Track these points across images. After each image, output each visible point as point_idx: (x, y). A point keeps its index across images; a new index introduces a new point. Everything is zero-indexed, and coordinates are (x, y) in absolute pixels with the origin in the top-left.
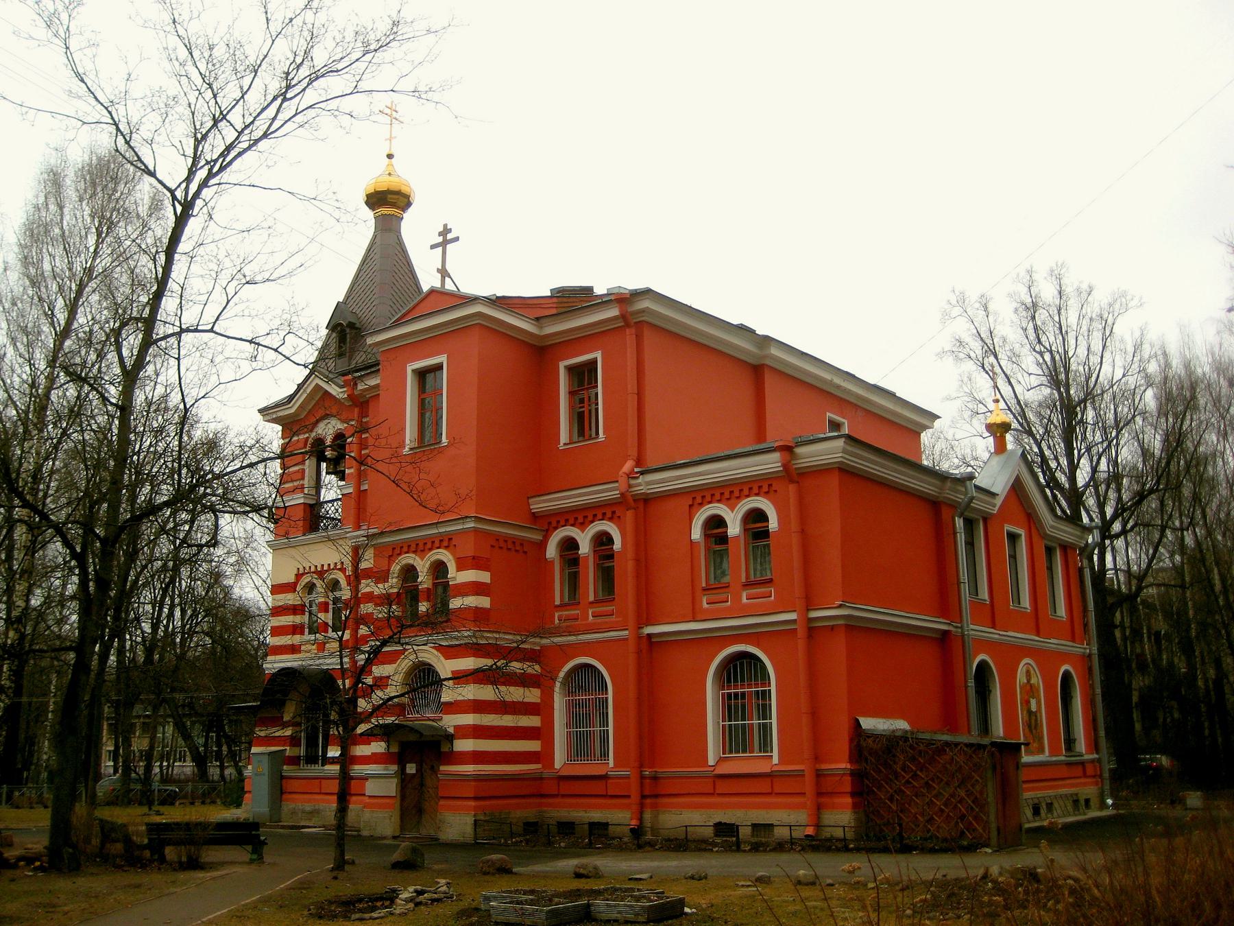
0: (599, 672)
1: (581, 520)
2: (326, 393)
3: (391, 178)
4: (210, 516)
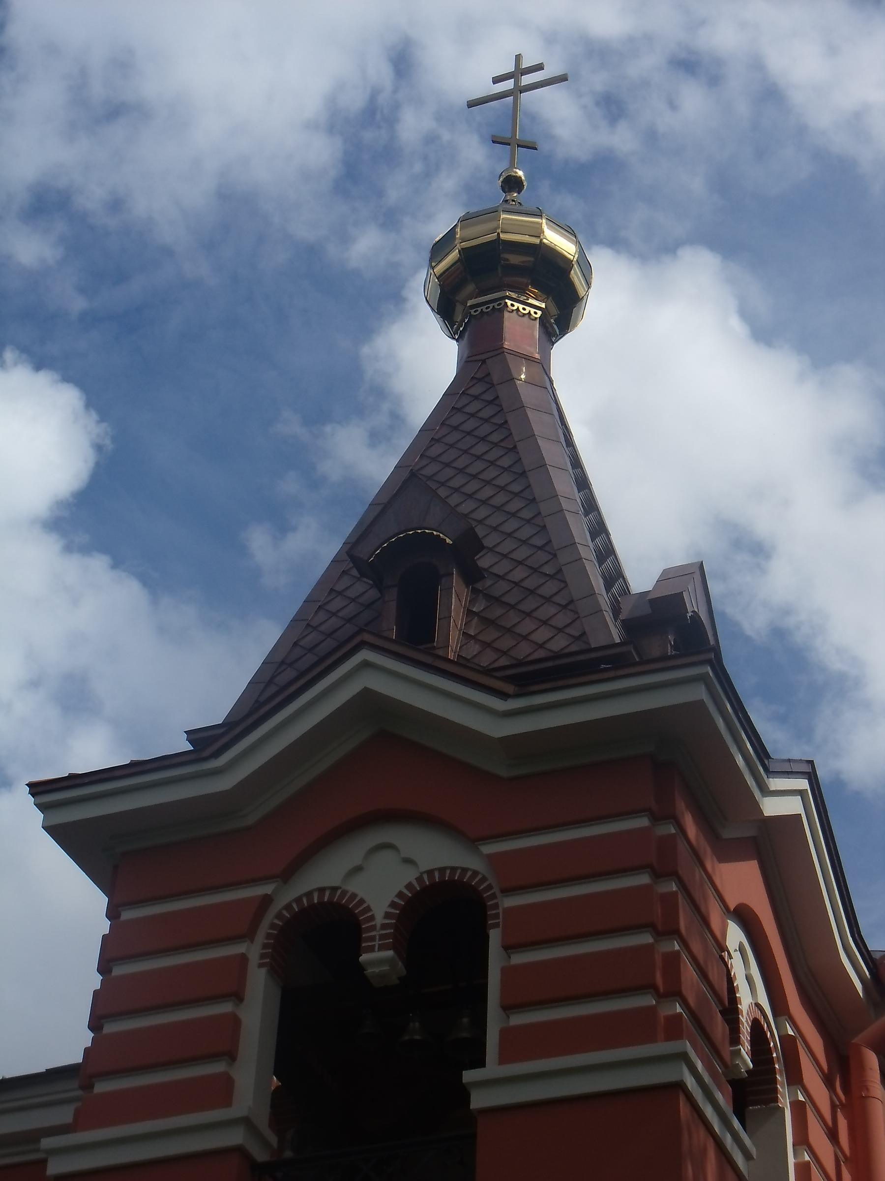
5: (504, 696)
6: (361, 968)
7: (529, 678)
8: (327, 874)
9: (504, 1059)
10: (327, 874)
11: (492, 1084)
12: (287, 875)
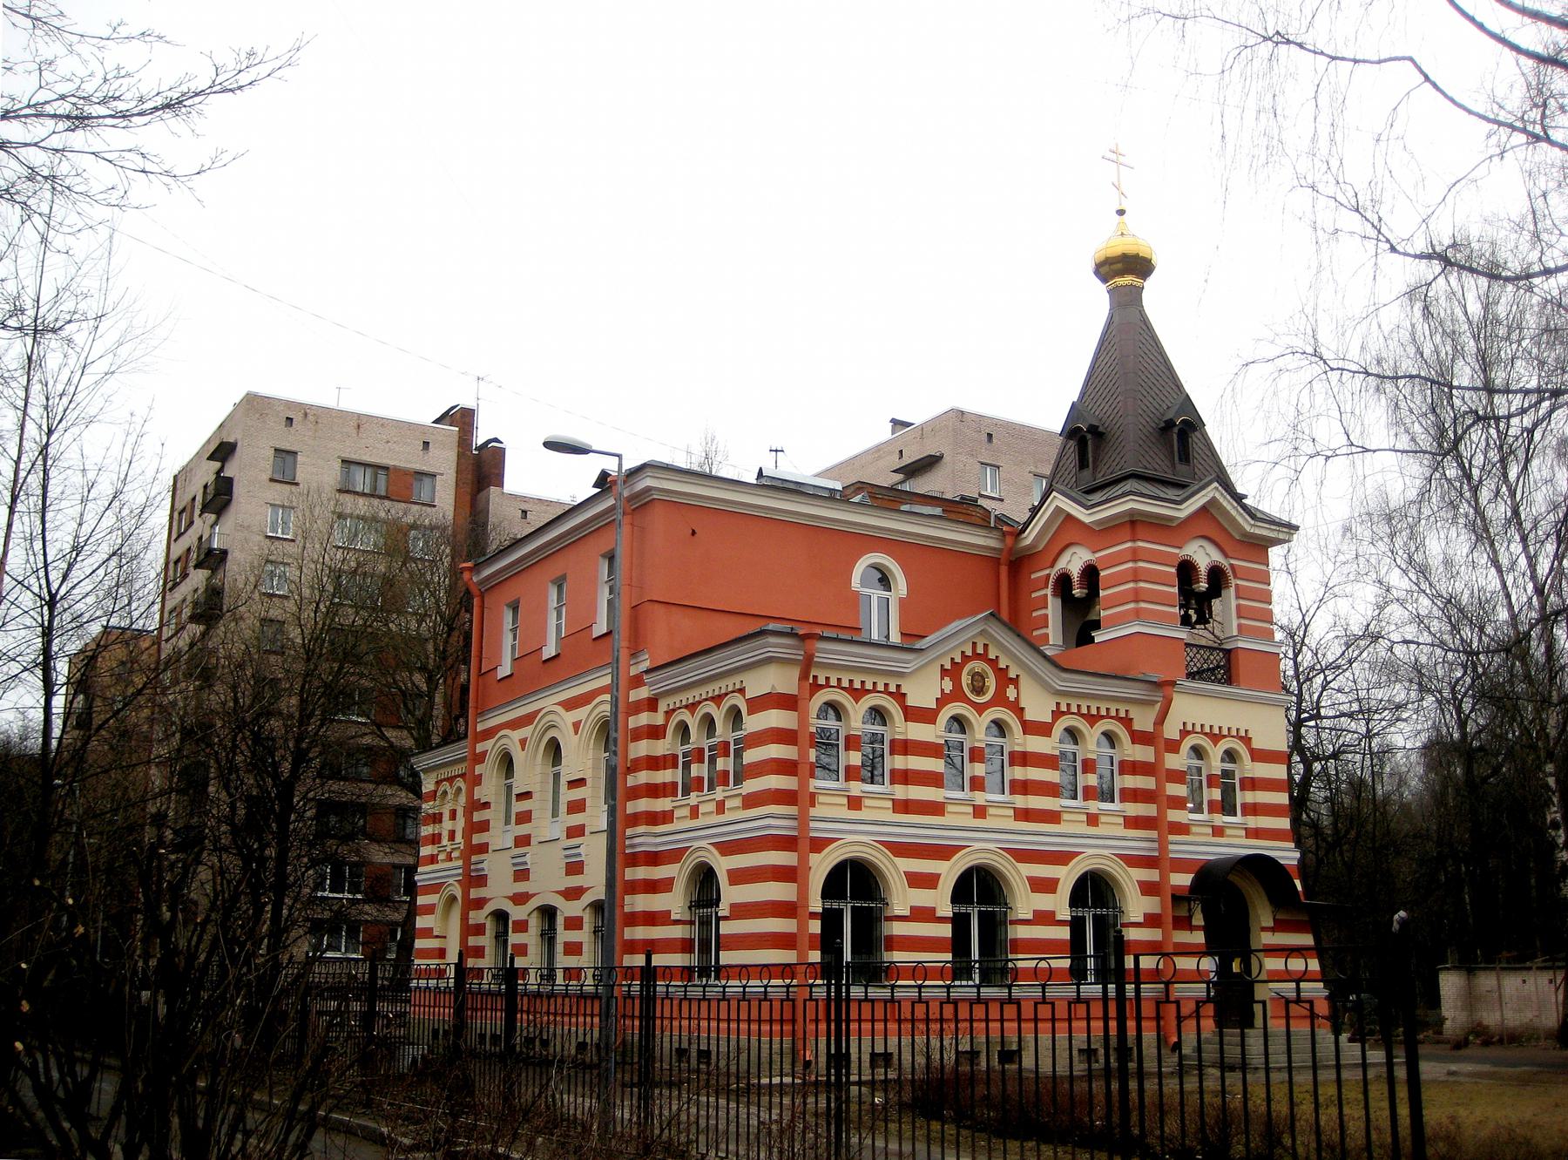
2: (1069, 517)
3: (1124, 239)
4: (1084, 1006)
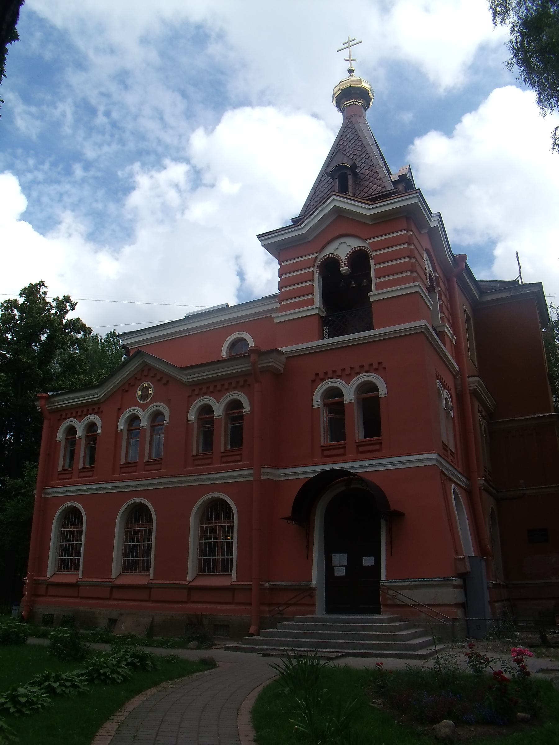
0: (227, 503)
1: (79, 414)
5: (369, 205)
6: (341, 271)
7: (374, 200)
8: (330, 250)
9: (377, 290)
10: (330, 250)
11: (374, 295)
12: (320, 252)
